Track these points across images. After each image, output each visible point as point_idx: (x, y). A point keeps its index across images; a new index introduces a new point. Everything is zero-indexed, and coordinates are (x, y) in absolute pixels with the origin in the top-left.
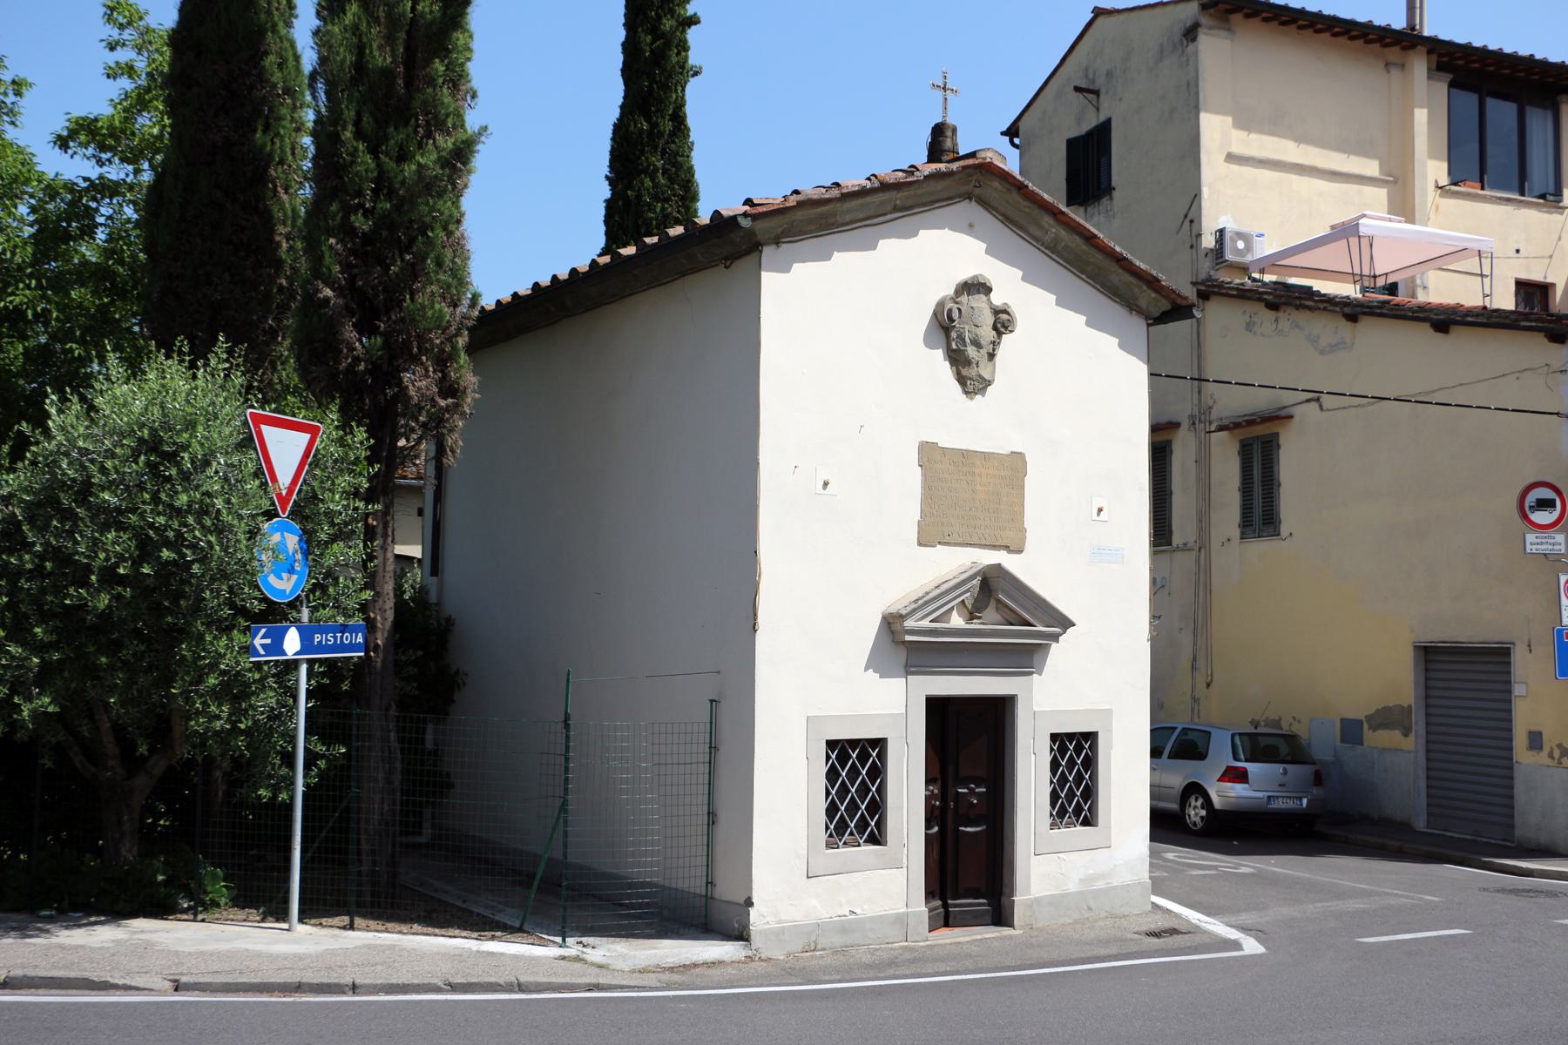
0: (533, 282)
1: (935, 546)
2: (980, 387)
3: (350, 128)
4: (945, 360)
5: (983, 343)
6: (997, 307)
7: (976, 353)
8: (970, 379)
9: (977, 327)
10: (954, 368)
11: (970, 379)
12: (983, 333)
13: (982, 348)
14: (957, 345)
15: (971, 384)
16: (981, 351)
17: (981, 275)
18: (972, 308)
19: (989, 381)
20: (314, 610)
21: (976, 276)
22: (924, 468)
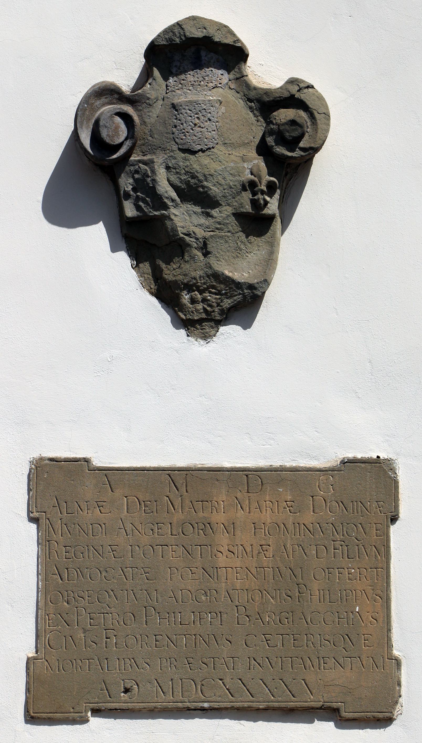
0: (113, 254)
1: (85, 721)
2: (227, 303)
3: (235, 165)
4: (114, 249)
5: (215, 190)
6: (267, 92)
7: (203, 220)
8: (189, 287)
9: (194, 153)
10: (146, 267)
11: (189, 287)
12: (214, 167)
13: (214, 204)
14: (138, 208)
15: (193, 301)
16: (215, 212)
17: (193, 18)
18: (174, 106)
19: (251, 287)
20: (116, 583)
21: (178, 24)
22: (43, 521)
